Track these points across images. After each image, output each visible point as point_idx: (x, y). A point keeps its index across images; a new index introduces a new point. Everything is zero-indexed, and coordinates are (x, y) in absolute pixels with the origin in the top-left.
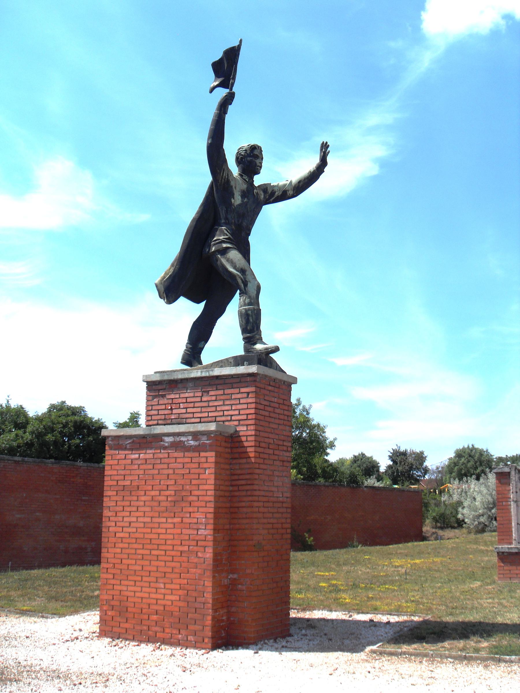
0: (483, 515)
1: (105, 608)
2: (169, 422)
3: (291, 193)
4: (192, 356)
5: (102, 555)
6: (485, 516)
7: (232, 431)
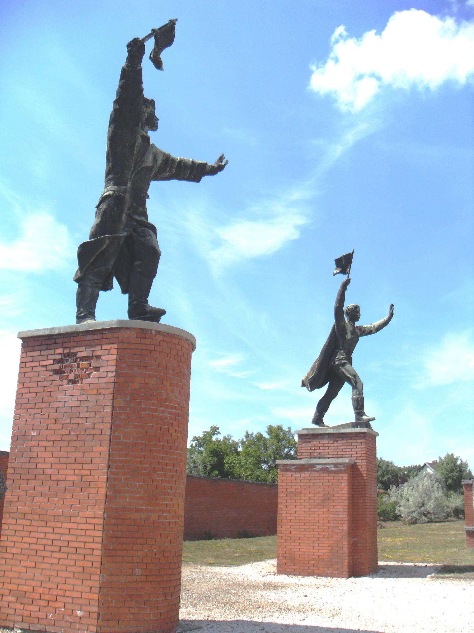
0: (414, 512)
1: (280, 558)
2: (313, 456)
3: (374, 331)
4: (318, 420)
5: (278, 529)
6: (416, 513)
7: (353, 462)
